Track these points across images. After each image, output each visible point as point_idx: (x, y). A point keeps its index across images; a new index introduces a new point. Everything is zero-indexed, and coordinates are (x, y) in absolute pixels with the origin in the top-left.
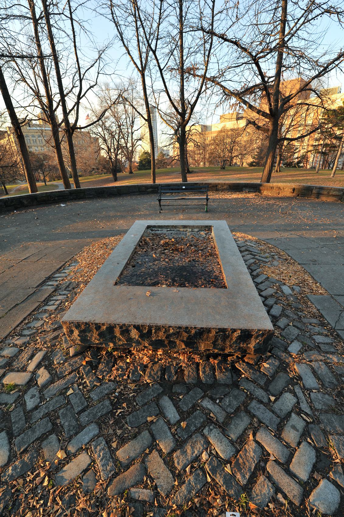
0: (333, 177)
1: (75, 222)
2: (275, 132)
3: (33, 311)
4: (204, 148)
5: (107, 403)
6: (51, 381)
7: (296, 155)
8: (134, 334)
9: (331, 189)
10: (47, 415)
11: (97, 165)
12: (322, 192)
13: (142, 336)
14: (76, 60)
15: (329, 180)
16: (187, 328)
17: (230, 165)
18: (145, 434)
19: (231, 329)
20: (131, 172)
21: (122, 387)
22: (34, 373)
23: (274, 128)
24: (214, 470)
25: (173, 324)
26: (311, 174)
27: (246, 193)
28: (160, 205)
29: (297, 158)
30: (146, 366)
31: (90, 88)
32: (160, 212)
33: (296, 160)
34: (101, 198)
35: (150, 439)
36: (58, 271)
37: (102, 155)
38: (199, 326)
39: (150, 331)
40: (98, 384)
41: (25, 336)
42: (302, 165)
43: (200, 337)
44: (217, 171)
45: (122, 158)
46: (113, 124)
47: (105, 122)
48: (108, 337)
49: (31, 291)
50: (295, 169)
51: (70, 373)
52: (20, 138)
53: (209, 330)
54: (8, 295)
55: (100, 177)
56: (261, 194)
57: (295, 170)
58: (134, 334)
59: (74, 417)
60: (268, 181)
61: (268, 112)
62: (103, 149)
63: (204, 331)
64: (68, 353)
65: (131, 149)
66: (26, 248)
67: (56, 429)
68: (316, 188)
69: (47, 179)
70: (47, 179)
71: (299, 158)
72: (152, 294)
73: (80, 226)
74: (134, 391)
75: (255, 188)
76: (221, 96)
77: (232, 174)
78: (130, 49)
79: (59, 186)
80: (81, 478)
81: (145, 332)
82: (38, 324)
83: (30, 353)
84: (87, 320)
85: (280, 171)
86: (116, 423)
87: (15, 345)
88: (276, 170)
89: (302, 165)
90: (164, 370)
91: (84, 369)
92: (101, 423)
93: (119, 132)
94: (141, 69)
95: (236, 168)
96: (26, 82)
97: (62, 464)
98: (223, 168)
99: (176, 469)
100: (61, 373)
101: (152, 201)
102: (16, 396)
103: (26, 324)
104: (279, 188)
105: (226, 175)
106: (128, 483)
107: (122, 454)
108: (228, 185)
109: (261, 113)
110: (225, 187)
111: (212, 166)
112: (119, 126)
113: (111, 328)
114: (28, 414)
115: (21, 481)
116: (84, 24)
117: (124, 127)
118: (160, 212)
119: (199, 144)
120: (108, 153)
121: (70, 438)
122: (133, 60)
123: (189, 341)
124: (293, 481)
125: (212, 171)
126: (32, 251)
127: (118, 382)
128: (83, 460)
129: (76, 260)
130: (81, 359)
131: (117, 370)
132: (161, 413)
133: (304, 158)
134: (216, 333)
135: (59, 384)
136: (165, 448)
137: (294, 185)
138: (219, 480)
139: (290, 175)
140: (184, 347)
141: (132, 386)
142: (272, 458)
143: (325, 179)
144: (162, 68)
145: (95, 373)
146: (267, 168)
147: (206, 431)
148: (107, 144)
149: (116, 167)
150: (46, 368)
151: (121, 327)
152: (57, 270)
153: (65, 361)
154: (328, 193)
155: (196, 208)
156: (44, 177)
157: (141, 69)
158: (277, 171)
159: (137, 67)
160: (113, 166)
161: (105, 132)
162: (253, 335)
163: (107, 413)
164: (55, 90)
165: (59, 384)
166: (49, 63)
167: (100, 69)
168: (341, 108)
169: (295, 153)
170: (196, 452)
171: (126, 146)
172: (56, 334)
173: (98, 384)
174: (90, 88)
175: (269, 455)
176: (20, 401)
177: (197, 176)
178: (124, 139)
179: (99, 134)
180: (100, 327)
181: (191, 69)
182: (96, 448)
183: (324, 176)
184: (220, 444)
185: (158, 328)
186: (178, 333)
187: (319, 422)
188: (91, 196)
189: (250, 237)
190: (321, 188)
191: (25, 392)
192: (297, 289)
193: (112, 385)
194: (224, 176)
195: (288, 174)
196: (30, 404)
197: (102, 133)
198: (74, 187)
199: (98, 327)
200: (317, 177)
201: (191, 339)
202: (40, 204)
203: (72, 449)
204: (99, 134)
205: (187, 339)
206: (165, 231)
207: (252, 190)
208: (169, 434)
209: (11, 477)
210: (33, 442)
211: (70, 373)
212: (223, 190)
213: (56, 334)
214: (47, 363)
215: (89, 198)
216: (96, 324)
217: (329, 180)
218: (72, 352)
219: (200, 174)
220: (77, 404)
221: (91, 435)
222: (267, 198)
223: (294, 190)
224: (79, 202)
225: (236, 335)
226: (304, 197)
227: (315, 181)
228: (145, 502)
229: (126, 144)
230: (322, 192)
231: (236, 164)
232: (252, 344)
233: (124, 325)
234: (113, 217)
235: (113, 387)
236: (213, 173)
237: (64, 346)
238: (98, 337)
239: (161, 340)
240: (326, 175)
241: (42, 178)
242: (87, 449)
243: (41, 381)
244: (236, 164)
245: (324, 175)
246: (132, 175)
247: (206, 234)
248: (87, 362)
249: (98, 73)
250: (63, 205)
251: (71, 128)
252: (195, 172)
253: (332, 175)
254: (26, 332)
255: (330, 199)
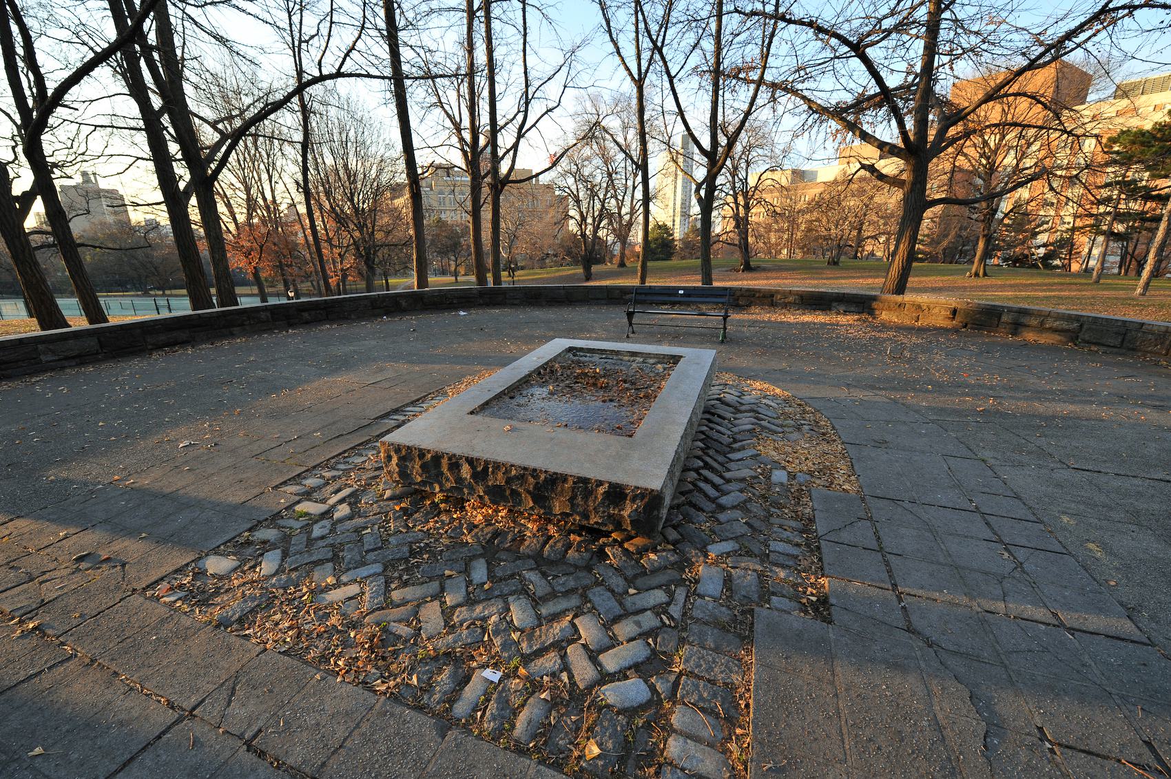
0: (1143, 294)
1: (471, 340)
2: (918, 186)
3: (359, 445)
4: (793, 223)
5: (406, 549)
6: (350, 518)
7: (1043, 238)
8: (466, 471)
9: (1049, 314)
10: (332, 545)
11: (555, 247)
12: (1025, 320)
13: (475, 475)
14: (523, 71)
15: (1128, 302)
16: (535, 470)
17: (856, 257)
18: (435, 585)
19: (596, 481)
20: (622, 264)
21: (432, 540)
22: (334, 506)
23: (915, 178)
24: (497, 632)
25: (517, 462)
26: (1076, 284)
27: (838, 313)
28: (631, 324)
29: (1044, 245)
30: (476, 526)
31: (546, 113)
32: (628, 337)
33: (1042, 251)
34: (533, 305)
35: (438, 589)
36: (413, 403)
37: (570, 229)
38: (552, 469)
39: (486, 469)
40: (404, 531)
41: (338, 470)
42: (1057, 262)
43: (552, 489)
44: (817, 268)
45: (607, 235)
46: (599, 171)
47: (583, 166)
48: (433, 472)
49: (366, 422)
50: (1035, 271)
51: (375, 515)
52: (416, 197)
53: (564, 478)
54: (334, 423)
55: (559, 271)
56: (874, 318)
57: (1032, 275)
58: (466, 471)
59: (360, 553)
60: (900, 288)
61: (899, 142)
62: (572, 217)
63: (557, 479)
64: (382, 496)
65: (627, 218)
66: (381, 370)
67: (335, 559)
68: (1010, 310)
69: (462, 270)
70: (462, 270)
71: (1052, 244)
72: (513, 429)
73: (475, 347)
74: (447, 546)
75: (862, 304)
76: (804, 116)
77: (854, 278)
78: (620, 45)
79: (468, 280)
80: (343, 603)
81: (479, 469)
82: (359, 460)
83: (336, 487)
84: (410, 444)
85: (985, 274)
86: (407, 570)
87: (322, 477)
88: (973, 270)
89: (1057, 262)
90: (496, 534)
91: (394, 514)
92: (389, 565)
93: (608, 186)
94: (636, 77)
95: (871, 262)
96: (442, 107)
97: (328, 588)
98: (834, 263)
99: (452, 620)
100: (366, 512)
101: (617, 316)
102: (305, 523)
103: (345, 457)
104: (919, 307)
105: (837, 278)
106: (391, 617)
107: (396, 595)
108: (797, 295)
109: (888, 147)
110: (791, 299)
111: (811, 257)
112: (610, 175)
113: (437, 458)
114: (310, 542)
115: (281, 591)
116: (550, 12)
117: (619, 177)
118: (628, 337)
119: (778, 210)
120: (581, 226)
121: (349, 569)
122: (624, 64)
123: (536, 492)
124: (593, 667)
125: (806, 268)
126: (390, 374)
127: (429, 534)
128: (353, 589)
129: (446, 393)
130: (396, 504)
131: (436, 522)
132: (466, 571)
133: (1066, 245)
134: (574, 483)
135: (358, 521)
136: (451, 601)
137: (952, 301)
138: (498, 641)
139: (1011, 286)
140: (531, 504)
141: (445, 541)
142: (582, 641)
143: (1117, 299)
144: (673, 74)
145: (406, 520)
146: (896, 262)
147: (511, 599)
148: (579, 208)
149: (591, 253)
150: (350, 504)
151: (450, 459)
152: (412, 403)
153: (377, 502)
154: (1042, 323)
155: (705, 335)
156: (457, 266)
157: (636, 77)
158: (977, 275)
159: (631, 74)
160: (586, 250)
161: (580, 186)
162: (627, 495)
163: (402, 559)
164: (485, 119)
165: (358, 521)
166: (481, 81)
167: (569, 78)
168: (1161, 128)
169: (1036, 234)
170: (486, 612)
171: (619, 214)
172: (377, 473)
173: (404, 531)
174: (546, 113)
175: (580, 637)
176: (307, 528)
177: (767, 279)
178: (617, 199)
179: (567, 190)
180: (424, 455)
181: (740, 70)
182: (372, 582)
183: (1116, 293)
184: (520, 613)
185: (497, 466)
186: (523, 476)
187: (684, 630)
188: (516, 302)
189: (778, 391)
190: (1023, 312)
191: (316, 522)
192: (801, 478)
193: (420, 535)
194: (832, 281)
195: (1008, 282)
196: (317, 531)
197: (574, 188)
198: (491, 285)
199: (422, 453)
200: (1094, 292)
201: (539, 489)
202: (427, 309)
203: (344, 578)
204: (567, 190)
205: (535, 488)
206: (596, 358)
207: (852, 309)
208: (463, 590)
209: (273, 586)
210: (306, 564)
211: (375, 515)
212: (786, 306)
213: (377, 473)
214: (352, 500)
215: (513, 305)
216: (420, 450)
217: (1128, 302)
218: (388, 493)
219: (774, 274)
220: (369, 542)
221: (372, 571)
222: (885, 326)
223: (954, 312)
224: (493, 311)
225: (601, 490)
226: (979, 330)
227: (1081, 304)
228: (401, 637)
229: (620, 209)
230: (1025, 320)
231: (872, 254)
232: (627, 511)
233: (454, 455)
234: (537, 338)
235: (420, 536)
236: (806, 273)
237: (381, 487)
238: (420, 471)
239: (500, 487)
240: (1123, 289)
241: (453, 269)
242: (360, 583)
243: (337, 515)
244: (872, 254)
245: (1115, 289)
246: (621, 269)
247: (665, 369)
248: (401, 508)
249: (565, 87)
250: (462, 313)
251: (501, 182)
252: (764, 270)
253: (1139, 291)
254: (342, 467)
255: (1046, 339)
